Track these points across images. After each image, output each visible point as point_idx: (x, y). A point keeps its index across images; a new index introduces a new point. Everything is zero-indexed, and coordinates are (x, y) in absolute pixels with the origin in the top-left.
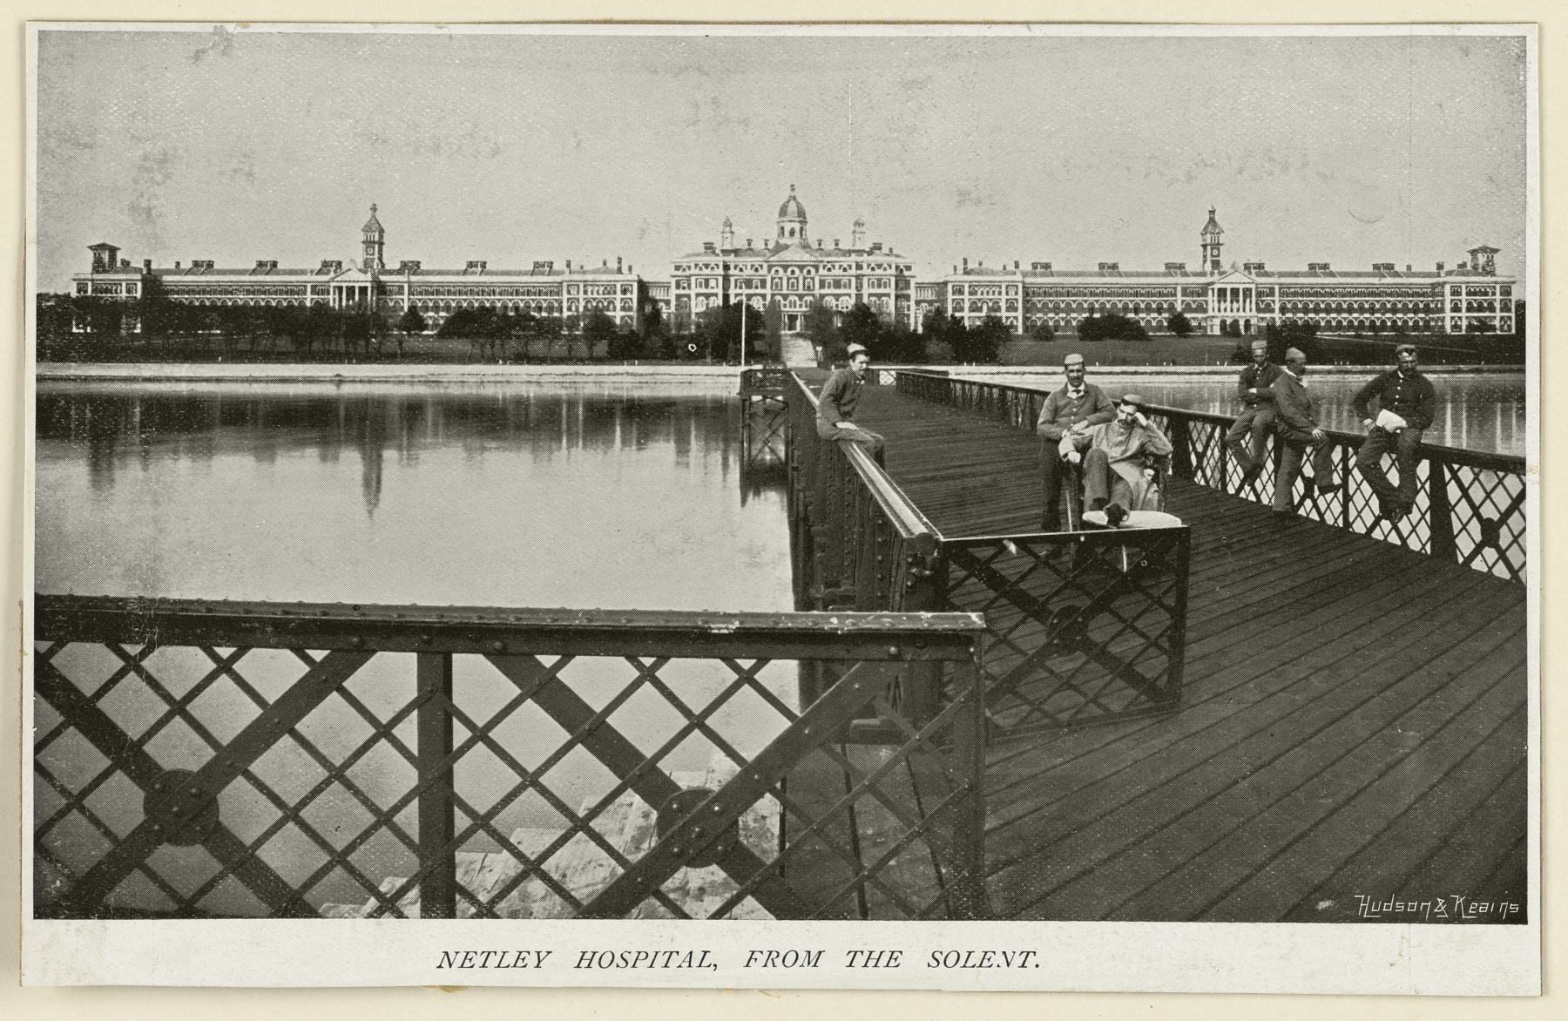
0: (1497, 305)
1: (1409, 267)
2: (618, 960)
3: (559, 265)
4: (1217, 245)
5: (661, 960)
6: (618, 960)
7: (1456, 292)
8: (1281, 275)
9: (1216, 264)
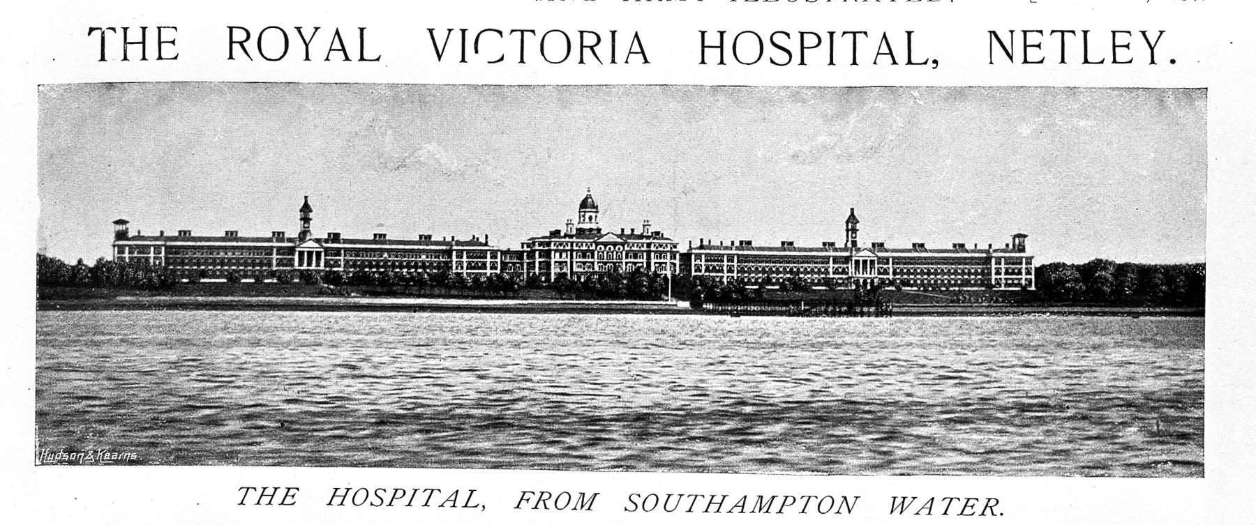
0: (1023, 271)
1: (162, 233)
2: (372, 498)
3: (969, 246)
4: (854, 230)
5: (421, 498)
6: (372, 498)
7: (998, 262)
8: (893, 251)
9: (854, 243)
